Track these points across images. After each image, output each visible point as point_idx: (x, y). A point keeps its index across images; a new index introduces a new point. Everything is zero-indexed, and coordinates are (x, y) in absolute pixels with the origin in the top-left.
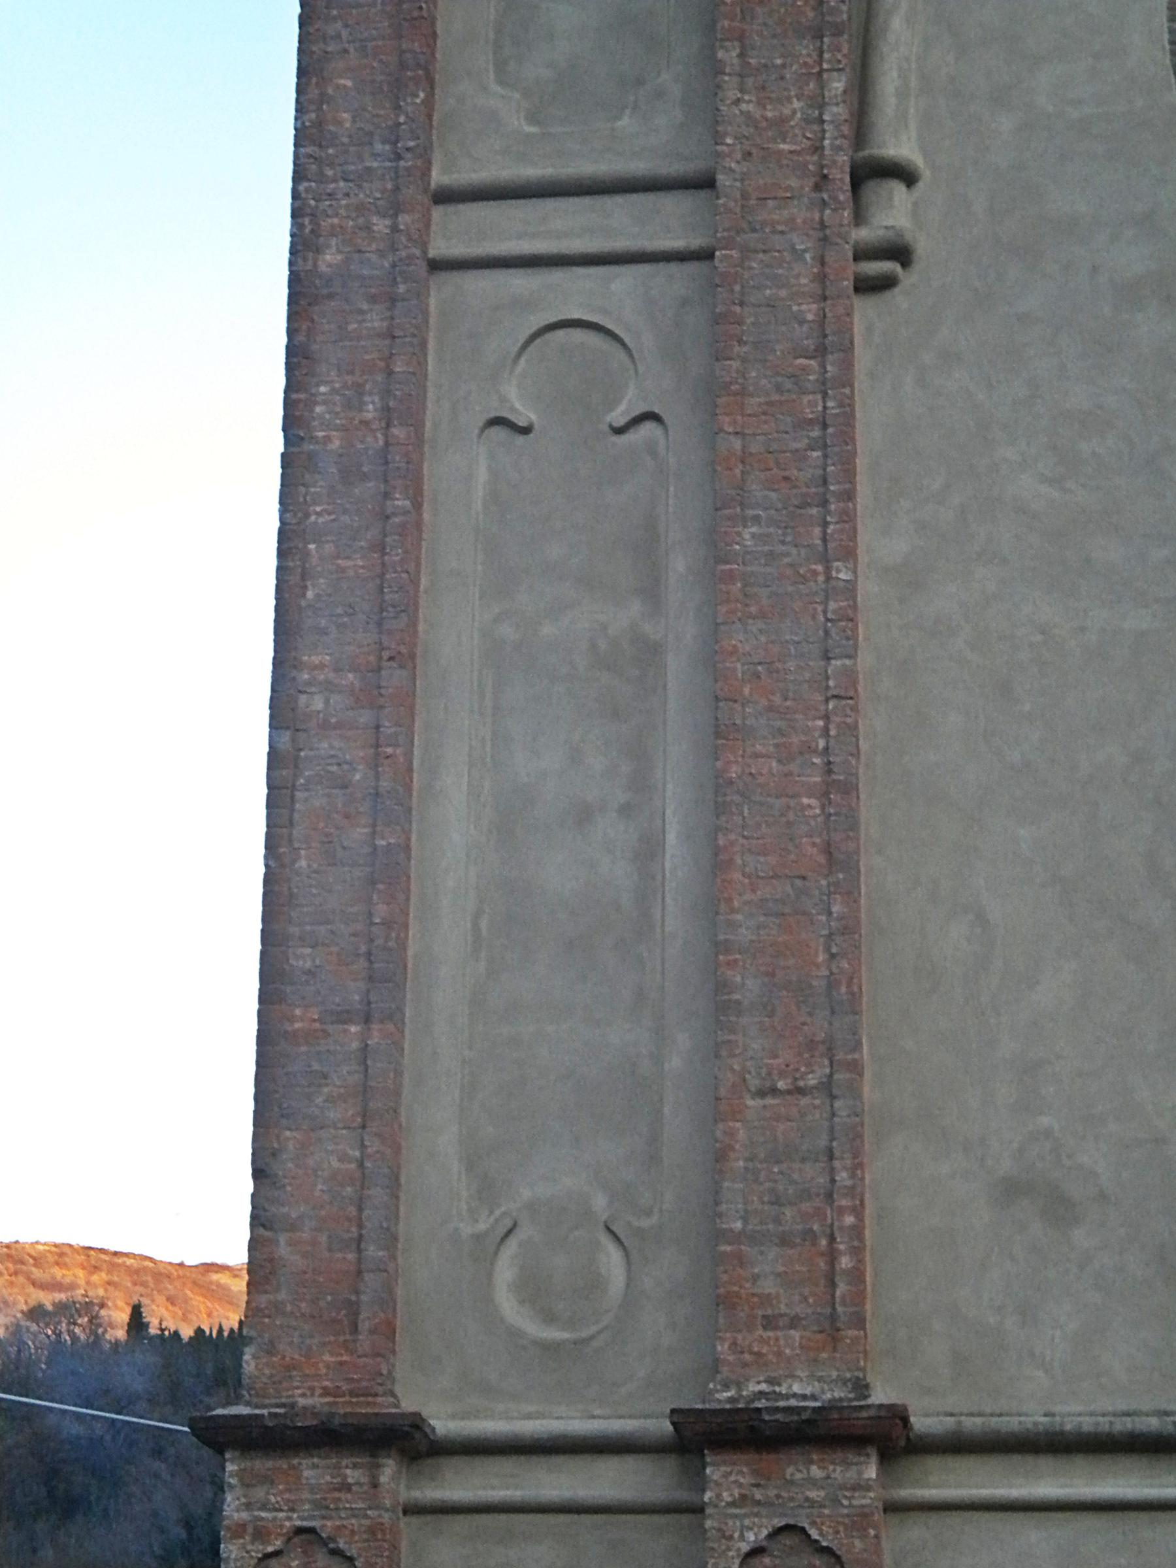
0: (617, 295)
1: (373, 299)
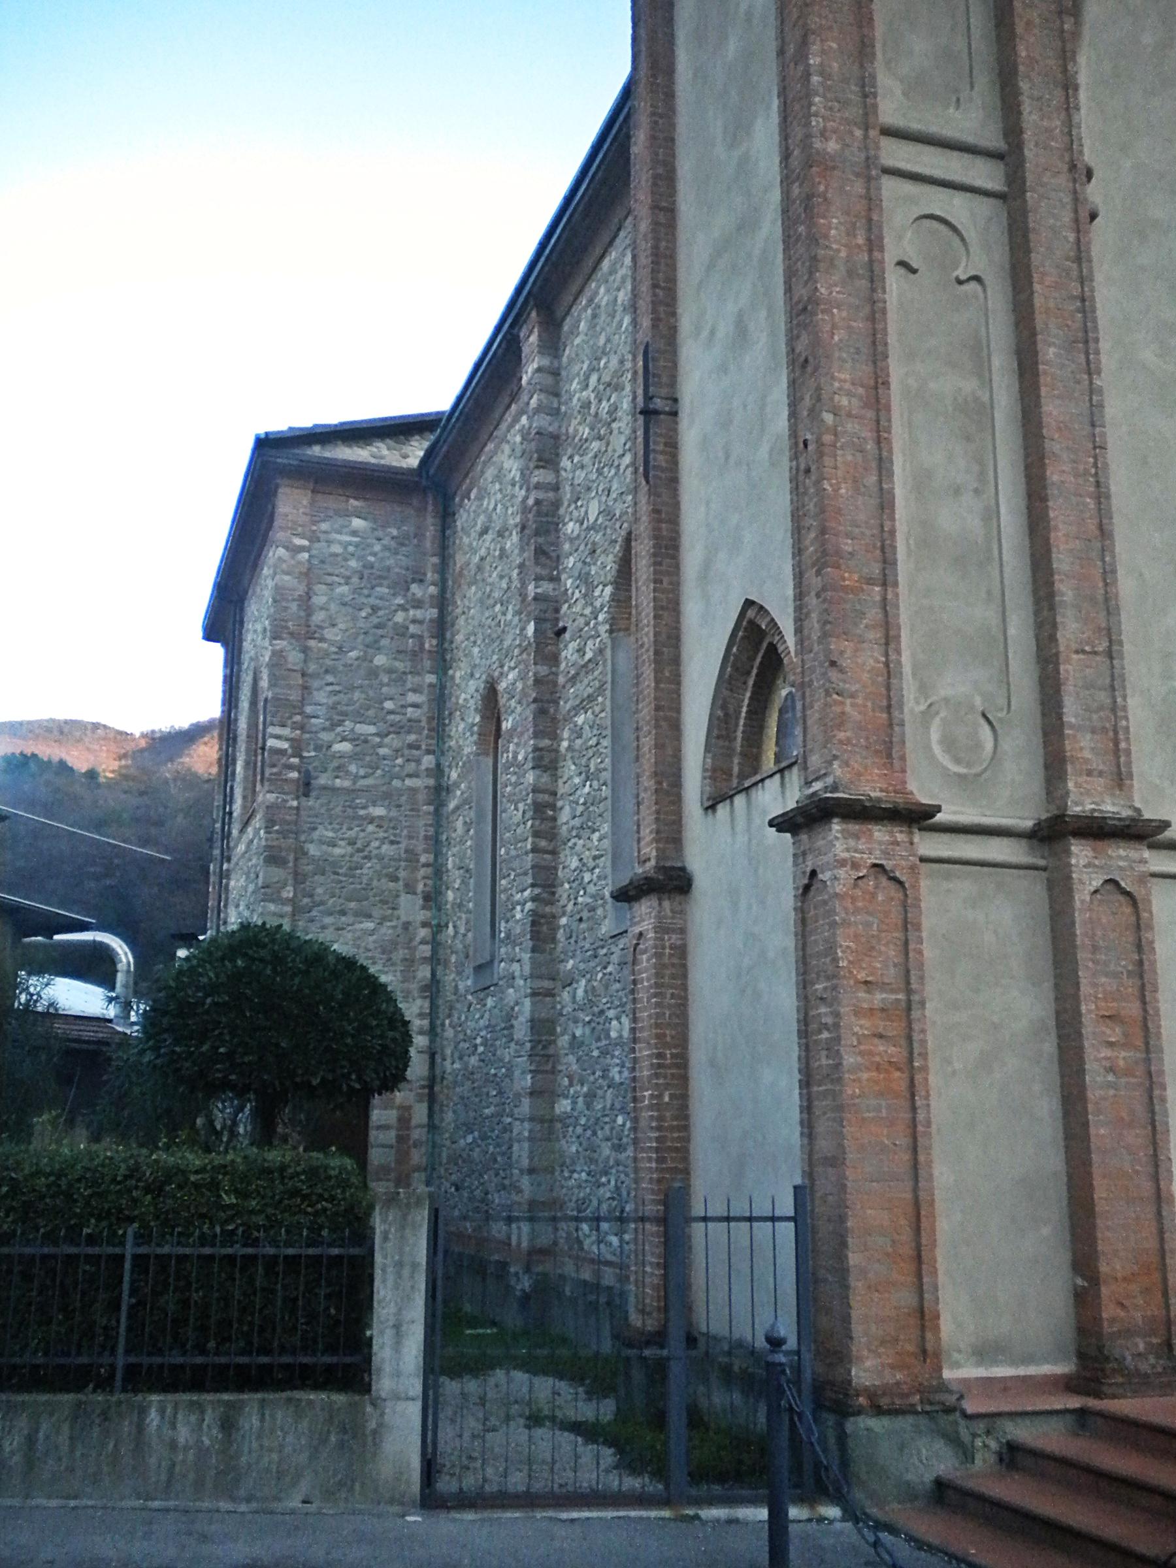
0: (957, 207)
1: (857, 175)
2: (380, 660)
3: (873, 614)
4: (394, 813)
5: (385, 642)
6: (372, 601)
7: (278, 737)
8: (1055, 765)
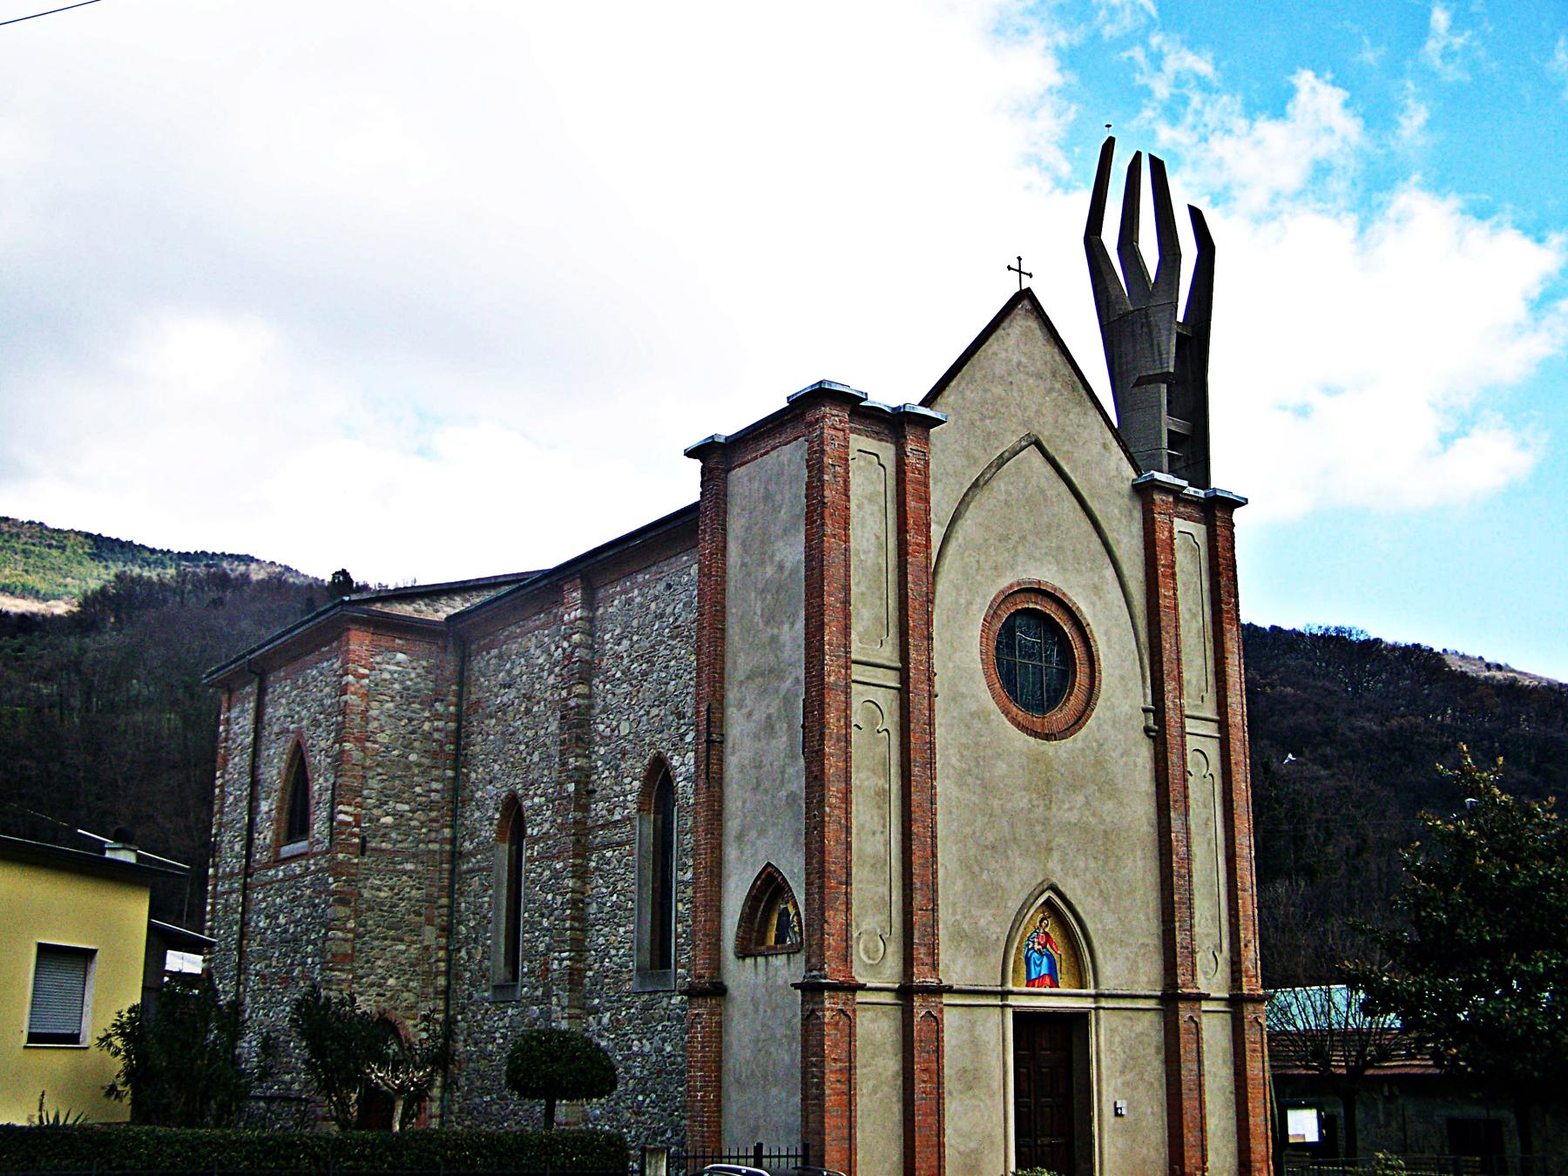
2: (413, 757)
3: (843, 897)
4: (420, 868)
5: (416, 744)
6: (409, 714)
7: (346, 813)
8: (908, 961)
